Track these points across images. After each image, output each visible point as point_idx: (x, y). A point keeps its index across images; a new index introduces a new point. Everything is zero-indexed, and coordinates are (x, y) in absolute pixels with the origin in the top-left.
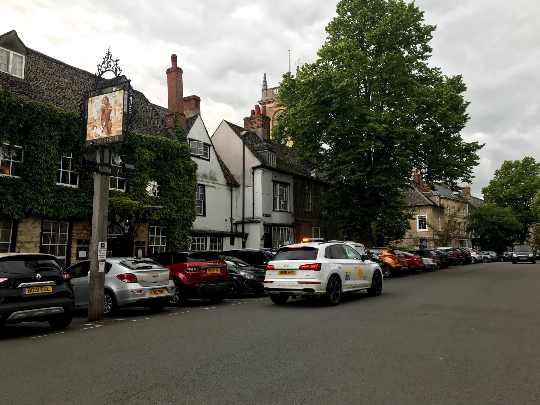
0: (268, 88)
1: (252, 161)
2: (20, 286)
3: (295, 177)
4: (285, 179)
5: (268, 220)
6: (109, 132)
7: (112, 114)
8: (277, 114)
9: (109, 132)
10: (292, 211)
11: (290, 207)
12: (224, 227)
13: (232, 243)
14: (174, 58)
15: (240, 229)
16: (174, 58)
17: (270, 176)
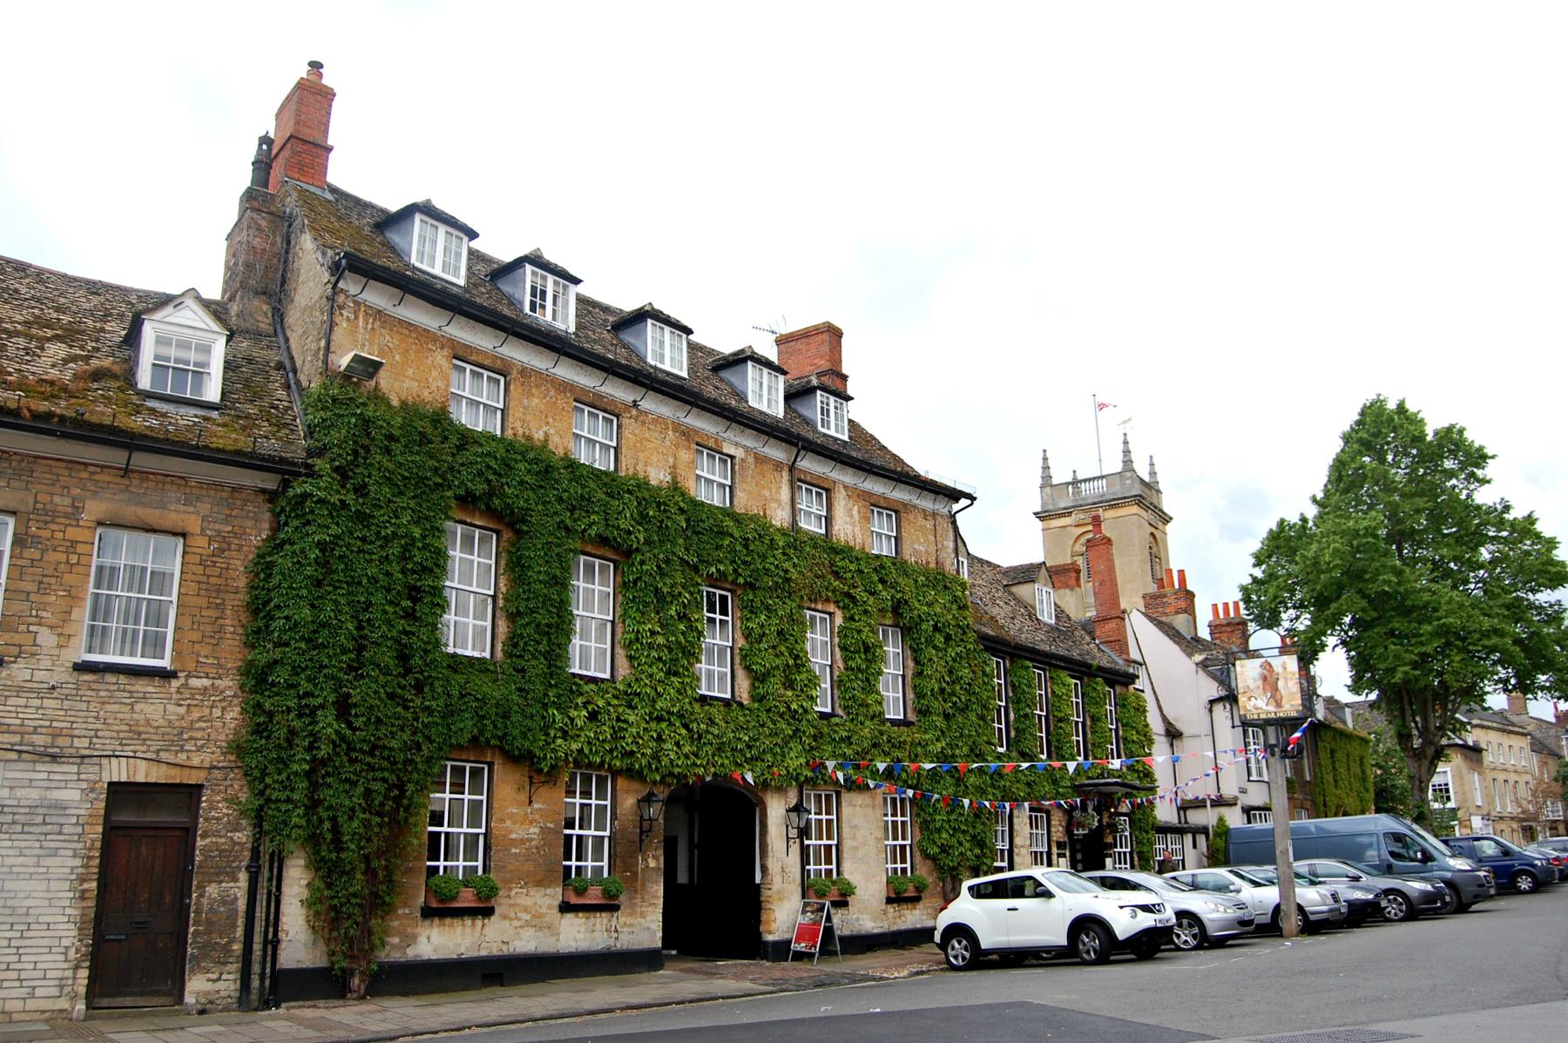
0: (1055, 481)
6: (1279, 705)
7: (1280, 684)
9: (1279, 705)
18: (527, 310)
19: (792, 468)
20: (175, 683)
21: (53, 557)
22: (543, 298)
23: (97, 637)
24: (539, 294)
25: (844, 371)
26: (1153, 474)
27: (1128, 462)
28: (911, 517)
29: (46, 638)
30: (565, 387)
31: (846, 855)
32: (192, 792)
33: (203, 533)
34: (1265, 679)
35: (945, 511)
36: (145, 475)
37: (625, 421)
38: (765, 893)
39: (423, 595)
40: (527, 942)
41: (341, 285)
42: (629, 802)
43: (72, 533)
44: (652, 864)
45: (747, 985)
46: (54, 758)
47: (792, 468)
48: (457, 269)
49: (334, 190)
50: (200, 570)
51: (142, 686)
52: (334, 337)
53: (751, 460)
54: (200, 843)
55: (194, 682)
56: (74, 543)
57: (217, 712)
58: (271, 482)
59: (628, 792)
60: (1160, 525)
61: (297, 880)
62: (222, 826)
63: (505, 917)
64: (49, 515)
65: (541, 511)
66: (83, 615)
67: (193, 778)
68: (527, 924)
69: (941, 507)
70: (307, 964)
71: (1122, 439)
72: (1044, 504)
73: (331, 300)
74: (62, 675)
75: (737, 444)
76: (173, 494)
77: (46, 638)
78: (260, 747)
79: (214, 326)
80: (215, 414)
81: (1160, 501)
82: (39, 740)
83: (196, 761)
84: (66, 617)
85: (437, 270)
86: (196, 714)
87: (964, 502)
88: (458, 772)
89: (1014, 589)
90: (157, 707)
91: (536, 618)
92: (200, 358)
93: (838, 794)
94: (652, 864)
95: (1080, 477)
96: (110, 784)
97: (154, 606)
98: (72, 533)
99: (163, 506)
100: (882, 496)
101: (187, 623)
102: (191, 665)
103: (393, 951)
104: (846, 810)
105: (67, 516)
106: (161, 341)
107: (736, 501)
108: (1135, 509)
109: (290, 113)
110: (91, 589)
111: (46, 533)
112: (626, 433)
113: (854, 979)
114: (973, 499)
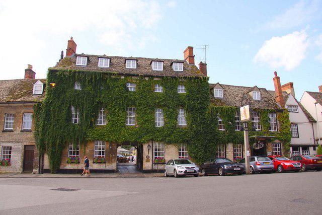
14: (276, 73)
16: (276, 73)
29: (18, 128)
46: (18, 142)
61: (46, 157)
62: (37, 151)
70: (143, 167)
71: (60, 54)
77: (18, 128)
103: (62, 167)
106: (36, 87)
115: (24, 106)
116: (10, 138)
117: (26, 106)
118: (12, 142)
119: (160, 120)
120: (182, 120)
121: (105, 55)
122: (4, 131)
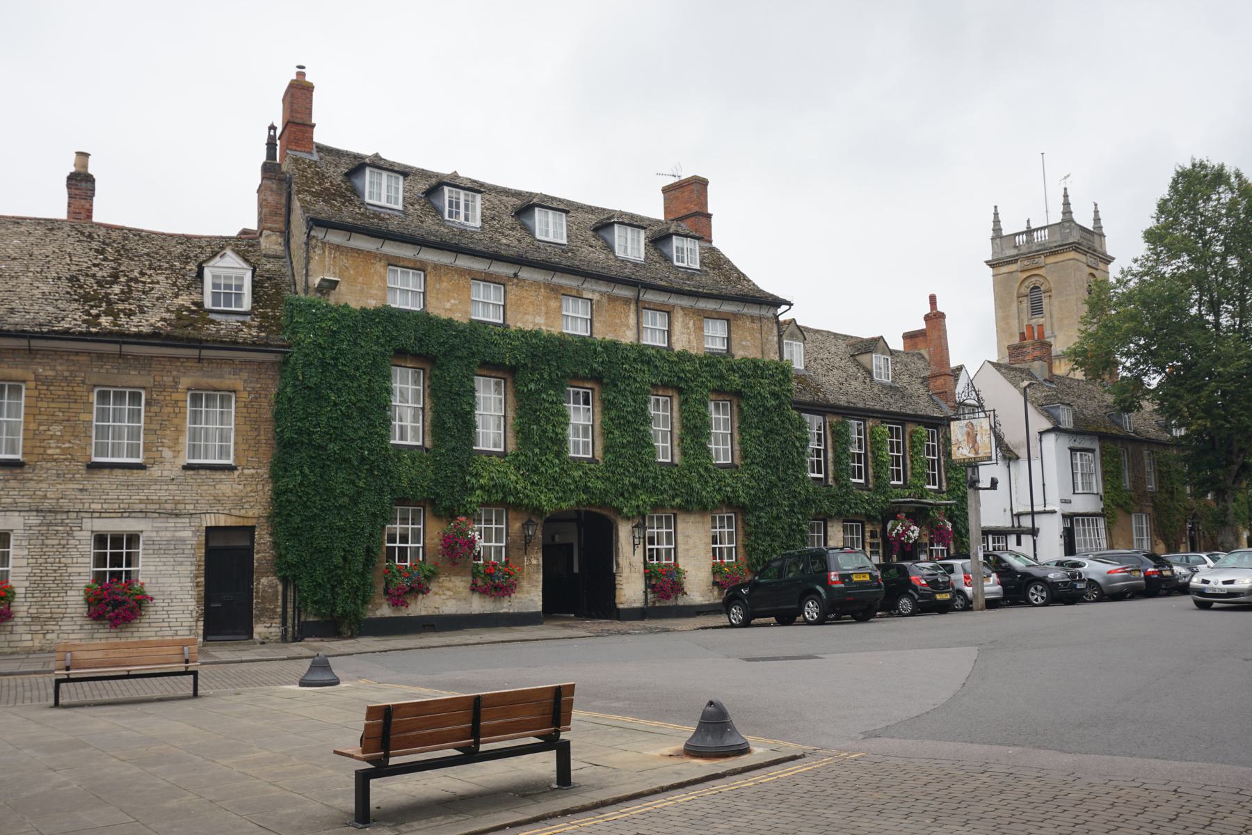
0: (1004, 233)
1: (1040, 422)
2: (819, 588)
3: (1102, 437)
4: (1086, 444)
5: (1069, 509)
6: (977, 453)
7: (978, 438)
8: (1026, 284)
9: (977, 453)
10: (1101, 492)
11: (1097, 485)
12: (1005, 522)
13: (1019, 543)
14: (933, 299)
15: (1026, 522)
16: (933, 299)
17: (1066, 442)
18: (446, 217)
19: (637, 301)
20: (236, 473)
21: (167, 410)
22: (458, 207)
23: (194, 451)
24: (454, 204)
25: (710, 211)
26: (1097, 220)
27: (1067, 211)
28: (740, 323)
29: (167, 453)
30: (463, 272)
31: (680, 555)
32: (251, 529)
33: (245, 389)
34: (968, 434)
35: (770, 314)
36: (210, 361)
37: (509, 288)
38: (618, 579)
39: (377, 408)
40: (450, 607)
41: (313, 233)
42: (516, 526)
43: (175, 396)
44: (534, 562)
45: (583, 633)
46: (177, 515)
47: (637, 301)
48: (397, 199)
49: (322, 149)
50: (244, 410)
51: (219, 475)
52: (311, 267)
53: (605, 300)
54: (256, 556)
55: (246, 471)
56: (177, 401)
57: (260, 487)
58: (279, 358)
59: (516, 519)
60: (1101, 266)
63: (436, 594)
64: (163, 387)
65: (449, 355)
66: (186, 440)
67: (249, 523)
68: (450, 598)
69: (767, 312)
72: (994, 253)
73: (307, 244)
74: (177, 472)
75: (593, 291)
76: (226, 369)
77: (167, 453)
78: (283, 507)
79: (245, 265)
80: (248, 319)
81: (1102, 245)
82: (169, 506)
83: (250, 514)
84: (176, 441)
85: (383, 203)
86: (249, 489)
87: (784, 308)
88: (405, 513)
89: (858, 358)
90: (228, 486)
91: (452, 417)
92: (238, 283)
93: (675, 515)
94: (534, 562)
95: (1033, 226)
96: (207, 528)
97: (197, 454)
98: (175, 396)
99: (222, 377)
100: (714, 311)
101: (240, 440)
102: (244, 463)
104: (680, 526)
105: (171, 387)
107: (595, 331)
108: (1072, 255)
109: (288, 98)
110: (188, 425)
111: (161, 398)
112: (510, 296)
113: (667, 631)
114: (790, 304)
115: (121, 355)
116: (135, 499)
117: (210, 361)
118: (145, 514)
119: (492, 417)
120: (722, 445)
121: (455, 175)
122: (93, 467)
